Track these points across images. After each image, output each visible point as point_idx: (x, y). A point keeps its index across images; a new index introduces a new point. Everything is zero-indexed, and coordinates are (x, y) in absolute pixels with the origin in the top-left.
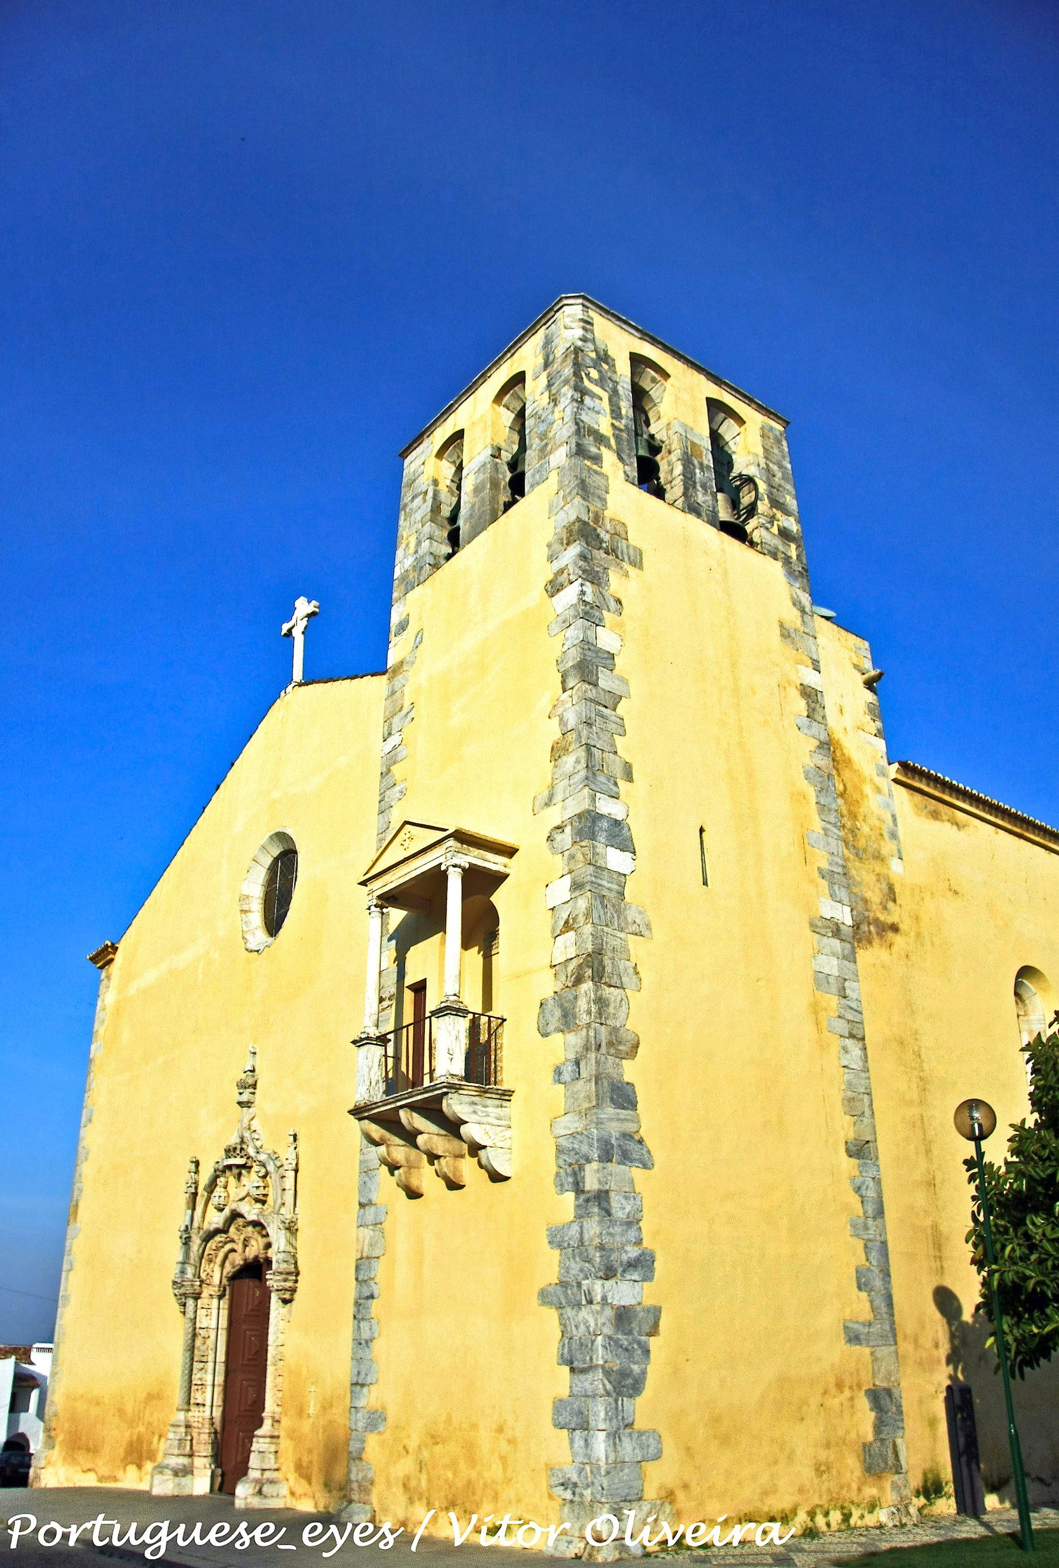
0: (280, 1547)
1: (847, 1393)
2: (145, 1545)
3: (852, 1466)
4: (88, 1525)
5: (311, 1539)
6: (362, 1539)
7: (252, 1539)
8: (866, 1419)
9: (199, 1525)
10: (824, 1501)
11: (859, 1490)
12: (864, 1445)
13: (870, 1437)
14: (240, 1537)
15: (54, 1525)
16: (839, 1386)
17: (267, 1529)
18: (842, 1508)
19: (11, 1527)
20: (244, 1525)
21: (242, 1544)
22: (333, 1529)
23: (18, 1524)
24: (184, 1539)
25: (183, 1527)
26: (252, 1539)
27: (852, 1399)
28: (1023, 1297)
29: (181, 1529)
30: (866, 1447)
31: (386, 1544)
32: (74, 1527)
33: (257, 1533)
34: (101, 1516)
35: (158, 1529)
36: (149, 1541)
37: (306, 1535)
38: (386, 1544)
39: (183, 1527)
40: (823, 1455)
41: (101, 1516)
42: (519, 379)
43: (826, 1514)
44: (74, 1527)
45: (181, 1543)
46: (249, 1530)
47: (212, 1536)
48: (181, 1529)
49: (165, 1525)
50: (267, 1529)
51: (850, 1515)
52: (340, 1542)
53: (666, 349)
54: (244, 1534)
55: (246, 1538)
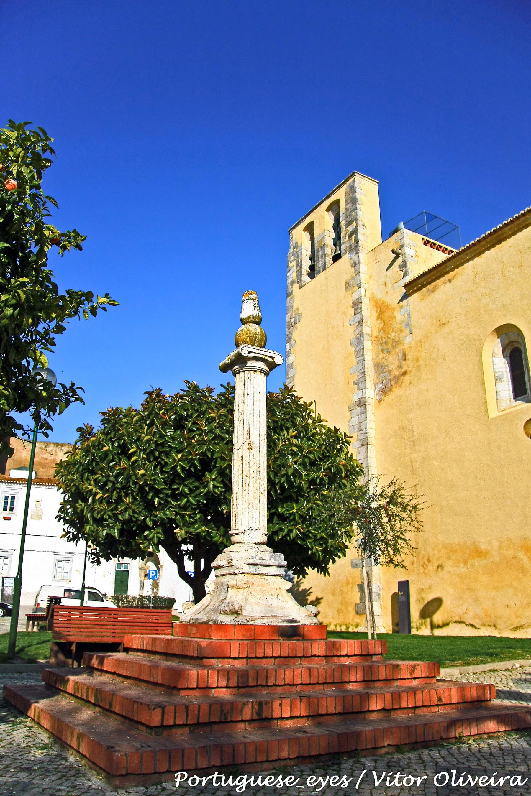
0: (297, 787)
1: (351, 586)
2: (236, 786)
3: (352, 611)
4: (211, 777)
5: (311, 783)
6: (334, 783)
7: (284, 783)
8: (356, 596)
9: (260, 777)
10: (339, 622)
11: (353, 620)
12: (356, 604)
13: (358, 602)
14: (279, 782)
15: (195, 777)
16: (348, 584)
17: (291, 779)
18: (346, 625)
19: (177, 778)
20: (281, 777)
21: (280, 786)
22: (321, 778)
23: (179, 776)
24: (254, 783)
25: (253, 778)
26: (284, 783)
27: (352, 588)
28: (44, 394)
29: (252, 779)
30: (356, 605)
31: (345, 785)
32: (204, 778)
33: (287, 780)
34: (217, 773)
35: (241, 779)
36: (238, 784)
37: (308, 782)
38: (345, 785)
39: (253, 778)
40: (340, 607)
41: (217, 773)
42: (337, 202)
43: (341, 626)
44: (204, 778)
45: (252, 785)
46: (283, 779)
47: (266, 782)
48: (252, 779)
49: (245, 777)
50: (291, 779)
51: (349, 627)
52: (324, 784)
53: (305, 217)
54: (281, 781)
55: (282, 783)
